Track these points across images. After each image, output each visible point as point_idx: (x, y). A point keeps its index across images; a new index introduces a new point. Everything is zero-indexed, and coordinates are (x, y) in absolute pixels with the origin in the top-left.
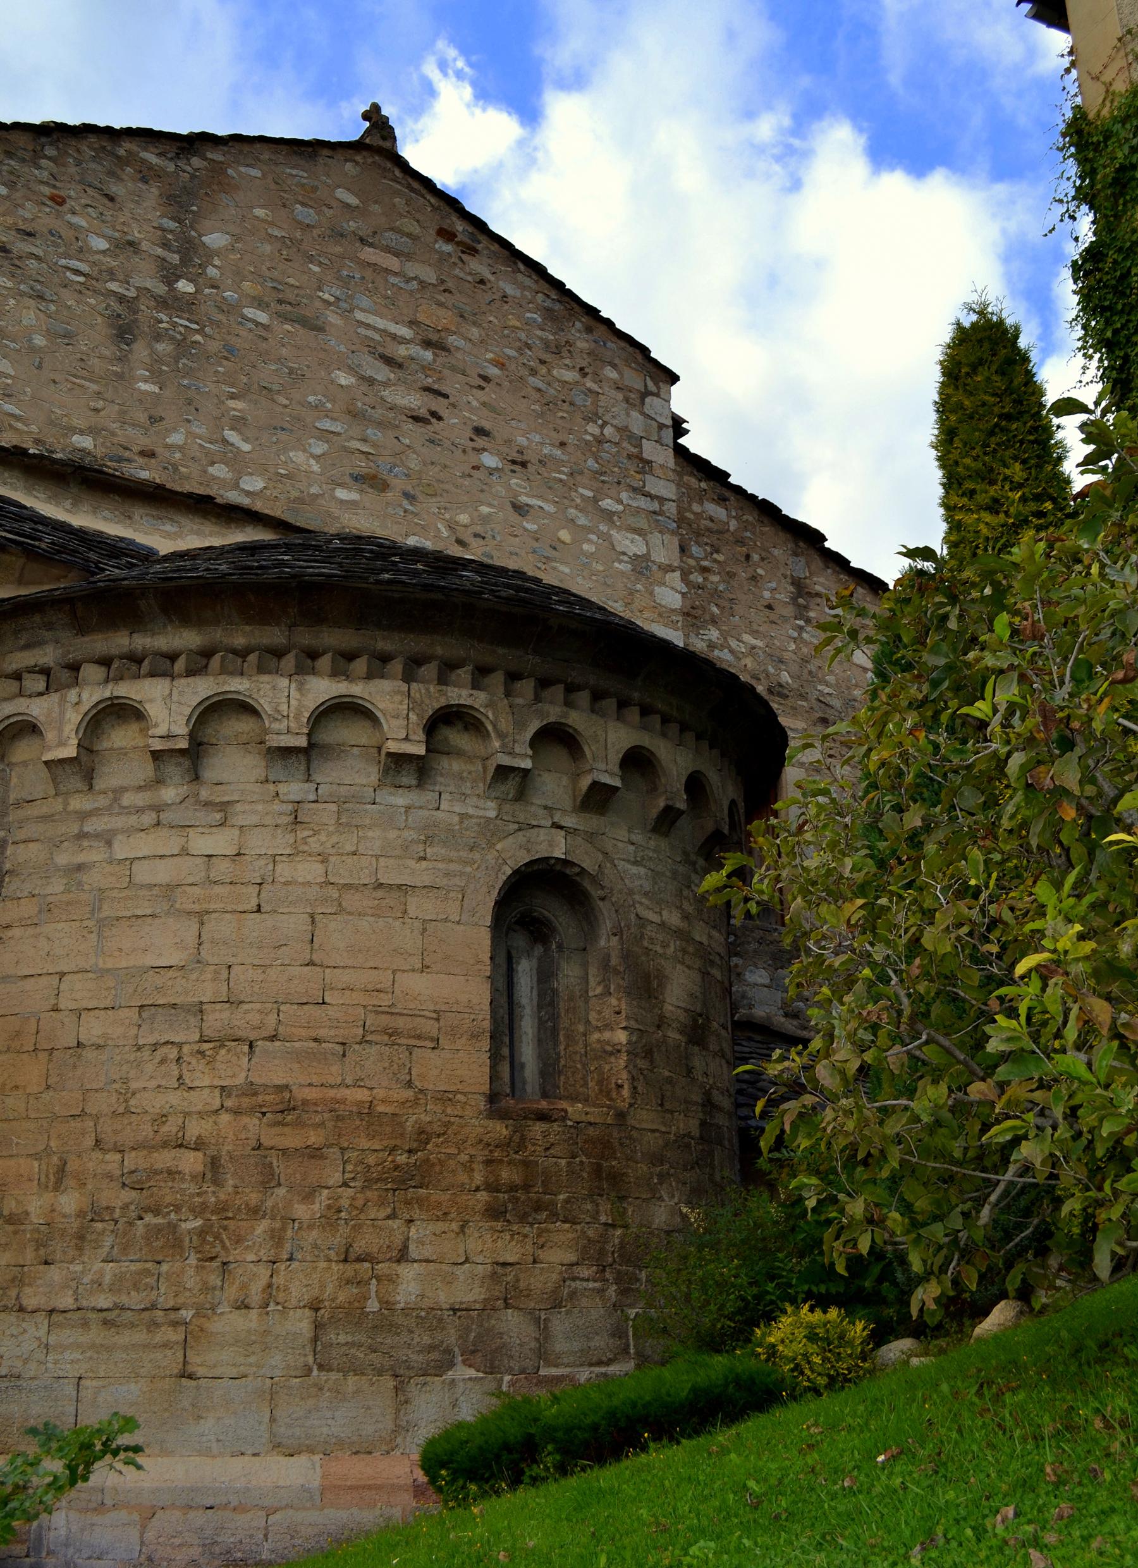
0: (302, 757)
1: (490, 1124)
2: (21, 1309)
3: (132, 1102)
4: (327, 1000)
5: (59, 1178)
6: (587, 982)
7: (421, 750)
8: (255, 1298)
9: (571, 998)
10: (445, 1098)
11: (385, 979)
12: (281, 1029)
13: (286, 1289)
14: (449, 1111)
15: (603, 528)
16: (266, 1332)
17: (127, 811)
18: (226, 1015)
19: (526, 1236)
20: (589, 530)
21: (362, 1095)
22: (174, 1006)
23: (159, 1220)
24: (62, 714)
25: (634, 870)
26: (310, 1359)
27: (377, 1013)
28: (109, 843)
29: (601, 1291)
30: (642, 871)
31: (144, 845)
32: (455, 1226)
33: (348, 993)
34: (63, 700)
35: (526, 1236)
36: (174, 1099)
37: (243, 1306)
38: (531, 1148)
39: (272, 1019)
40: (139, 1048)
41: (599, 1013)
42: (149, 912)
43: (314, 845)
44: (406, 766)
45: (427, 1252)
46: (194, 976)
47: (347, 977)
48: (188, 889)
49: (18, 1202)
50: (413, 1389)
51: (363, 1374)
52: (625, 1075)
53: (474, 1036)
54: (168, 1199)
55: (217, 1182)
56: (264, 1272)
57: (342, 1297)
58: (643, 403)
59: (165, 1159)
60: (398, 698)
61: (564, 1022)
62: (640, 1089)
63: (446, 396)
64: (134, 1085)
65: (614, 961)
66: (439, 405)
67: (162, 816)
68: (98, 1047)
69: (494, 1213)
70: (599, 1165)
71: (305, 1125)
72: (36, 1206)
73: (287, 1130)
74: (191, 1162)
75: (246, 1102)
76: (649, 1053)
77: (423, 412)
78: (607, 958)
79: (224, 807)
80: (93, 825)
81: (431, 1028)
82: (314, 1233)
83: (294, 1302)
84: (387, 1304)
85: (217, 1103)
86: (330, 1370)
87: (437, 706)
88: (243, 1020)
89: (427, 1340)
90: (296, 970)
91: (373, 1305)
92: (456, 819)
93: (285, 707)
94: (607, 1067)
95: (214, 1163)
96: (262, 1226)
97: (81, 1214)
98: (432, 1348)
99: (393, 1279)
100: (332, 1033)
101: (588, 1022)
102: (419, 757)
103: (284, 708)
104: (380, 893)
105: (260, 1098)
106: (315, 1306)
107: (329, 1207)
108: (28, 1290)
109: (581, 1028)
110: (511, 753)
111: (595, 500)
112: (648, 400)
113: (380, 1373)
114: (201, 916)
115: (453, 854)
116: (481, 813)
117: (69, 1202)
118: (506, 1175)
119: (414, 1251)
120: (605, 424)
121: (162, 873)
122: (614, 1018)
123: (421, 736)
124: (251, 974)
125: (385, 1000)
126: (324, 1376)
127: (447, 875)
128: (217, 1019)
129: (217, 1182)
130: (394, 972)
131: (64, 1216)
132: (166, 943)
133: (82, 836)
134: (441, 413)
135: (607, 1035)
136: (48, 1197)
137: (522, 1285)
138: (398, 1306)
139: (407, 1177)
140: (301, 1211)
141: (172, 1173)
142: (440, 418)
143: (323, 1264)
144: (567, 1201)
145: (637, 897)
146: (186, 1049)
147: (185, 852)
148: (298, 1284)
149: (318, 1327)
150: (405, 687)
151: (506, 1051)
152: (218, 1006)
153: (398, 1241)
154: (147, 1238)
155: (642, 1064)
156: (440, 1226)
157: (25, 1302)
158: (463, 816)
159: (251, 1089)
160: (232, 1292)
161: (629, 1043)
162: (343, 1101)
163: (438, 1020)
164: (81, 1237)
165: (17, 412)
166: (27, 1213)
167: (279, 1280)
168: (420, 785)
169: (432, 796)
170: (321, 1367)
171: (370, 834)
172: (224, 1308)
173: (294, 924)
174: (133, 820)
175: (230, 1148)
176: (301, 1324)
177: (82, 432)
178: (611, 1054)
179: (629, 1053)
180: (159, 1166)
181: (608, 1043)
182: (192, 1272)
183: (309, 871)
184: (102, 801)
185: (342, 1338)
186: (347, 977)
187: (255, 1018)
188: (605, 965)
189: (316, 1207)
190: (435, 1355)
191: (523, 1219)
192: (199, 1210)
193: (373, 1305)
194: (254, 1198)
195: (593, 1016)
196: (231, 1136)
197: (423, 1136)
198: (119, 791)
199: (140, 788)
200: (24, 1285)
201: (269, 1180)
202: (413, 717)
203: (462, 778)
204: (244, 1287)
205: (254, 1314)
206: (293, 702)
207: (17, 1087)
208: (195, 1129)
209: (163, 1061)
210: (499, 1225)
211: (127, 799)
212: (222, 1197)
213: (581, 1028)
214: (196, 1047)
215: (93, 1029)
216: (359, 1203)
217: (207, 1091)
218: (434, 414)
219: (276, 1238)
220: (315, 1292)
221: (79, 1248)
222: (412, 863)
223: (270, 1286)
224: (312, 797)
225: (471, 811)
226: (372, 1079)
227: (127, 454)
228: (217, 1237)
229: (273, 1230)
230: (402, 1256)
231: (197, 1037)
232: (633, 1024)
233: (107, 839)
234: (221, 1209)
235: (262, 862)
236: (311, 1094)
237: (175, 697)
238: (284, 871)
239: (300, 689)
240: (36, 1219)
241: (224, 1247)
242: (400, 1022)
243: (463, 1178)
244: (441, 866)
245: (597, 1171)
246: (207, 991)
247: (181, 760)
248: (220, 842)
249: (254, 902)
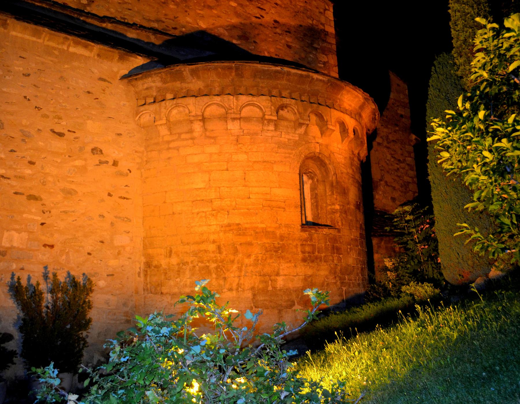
0: (238, 121)
1: (302, 234)
2: (162, 293)
3: (192, 230)
4: (251, 197)
5: (170, 254)
6: (326, 191)
7: (276, 118)
8: (234, 286)
9: (321, 196)
10: (287, 226)
11: (267, 190)
12: (237, 206)
13: (244, 284)
14: (289, 230)
15: (314, 52)
16: (239, 297)
17: (184, 140)
18: (219, 202)
19: (314, 267)
20: (310, 53)
21: (263, 226)
22: (203, 200)
23: (203, 264)
24: (160, 110)
25: (339, 156)
26: (252, 305)
27: (266, 200)
28: (178, 150)
29: (335, 283)
30: (342, 156)
31: (189, 151)
32: (293, 265)
33: (257, 195)
34: (160, 106)
35: (314, 267)
36: (205, 228)
37: (231, 290)
38: (314, 241)
39: (234, 203)
40: (193, 213)
41: (330, 200)
42: (192, 171)
43: (244, 149)
44: (271, 123)
45: (286, 272)
46: (208, 191)
47: (256, 190)
48: (205, 164)
49: (158, 261)
50: (283, 313)
51: (268, 308)
52: (339, 219)
53: (296, 207)
54: (205, 259)
55: (220, 253)
56: (237, 280)
57: (261, 286)
58: (325, 13)
59: (203, 247)
60: (268, 102)
61: (320, 203)
62: (344, 223)
63: (265, 10)
64: (193, 225)
65: (334, 185)
66: (263, 13)
67: (195, 141)
68: (179, 214)
69: (304, 260)
70: (333, 246)
71: (246, 235)
72: (164, 262)
73: (240, 237)
74: (212, 247)
75: (227, 229)
76: (345, 212)
77: (258, 15)
78: (332, 183)
79: (214, 138)
80: (172, 145)
81: (283, 205)
82: (251, 267)
83: (246, 288)
84: (274, 288)
85: (218, 229)
86: (258, 308)
87: (280, 104)
88: (226, 203)
89: (287, 298)
90: (240, 188)
91: (270, 288)
92: (287, 140)
93: (232, 105)
94: (333, 217)
95: (219, 248)
96: (235, 267)
97: (178, 264)
98: (289, 300)
99: (276, 281)
100: (253, 207)
101: (326, 203)
102: (275, 120)
103: (232, 105)
104: (265, 164)
105: (232, 227)
106: (253, 288)
107: (255, 259)
108: (163, 288)
109: (325, 205)
110: (303, 119)
111: (312, 44)
112: (326, 12)
113: (273, 308)
114: (209, 172)
115: (286, 151)
116: (294, 138)
117: (174, 261)
118: (307, 249)
119: (281, 272)
120: (314, 19)
121: (196, 159)
122: (335, 201)
123: (275, 114)
124: (226, 189)
125: (268, 197)
126: (257, 309)
127: (285, 158)
128: (217, 203)
129: (220, 253)
130: (271, 188)
131: (173, 265)
132: (199, 182)
133: (169, 149)
134: (263, 15)
135: (333, 207)
136: (167, 260)
137: (313, 281)
138: (278, 289)
139: (278, 250)
140: (247, 261)
141: (206, 251)
142: (263, 17)
143: (254, 277)
144: (325, 256)
145: (340, 164)
146: (208, 213)
147: (203, 152)
148: (247, 283)
149: (254, 295)
150: (269, 98)
151: (303, 212)
152: (217, 200)
153: (276, 269)
154: (200, 271)
155: (344, 215)
156: (289, 265)
157: (163, 291)
158: (289, 140)
159: (229, 225)
160: (227, 286)
161: (340, 209)
162: (257, 228)
163: (285, 202)
164: (179, 271)
165: (37, 58)
166: (161, 265)
167: (242, 282)
168: (276, 130)
169: (279, 133)
170: (256, 307)
171: (261, 145)
172: (225, 290)
173: (238, 174)
174: (185, 143)
175: (224, 243)
176: (249, 295)
177: (153, 21)
178: (335, 213)
179: (340, 212)
180: (202, 249)
181: (334, 209)
182: (214, 280)
183: (242, 157)
184: (175, 137)
185: (262, 298)
186: (256, 190)
187: (228, 203)
188: (332, 186)
189: (252, 259)
190: (290, 303)
191: (313, 261)
192: (216, 261)
193: (270, 288)
194: (232, 257)
195: (328, 201)
196: (224, 239)
197: (282, 238)
198: (180, 134)
199: (187, 133)
200: (162, 286)
201: (236, 251)
202: (273, 108)
203: (288, 127)
204: (231, 284)
205: (234, 292)
206: (235, 104)
207: (154, 227)
208: (212, 237)
209: (201, 217)
210: (306, 264)
211: (183, 136)
212: (222, 257)
213: (325, 205)
214: (211, 212)
215: (178, 208)
216: (264, 258)
217: (215, 226)
218: (261, 16)
219: (240, 269)
220: (252, 285)
221: (179, 275)
222: (274, 154)
223: (238, 284)
224: (242, 134)
225: (291, 138)
226: (263, 221)
227: (168, 28)
228: (222, 270)
229: (238, 267)
230: (278, 274)
231: (210, 209)
232: (341, 204)
233: (177, 149)
234: (222, 261)
235: (227, 155)
236: (247, 226)
237: (197, 103)
238: (235, 157)
239: (237, 100)
240: (164, 266)
241: (224, 272)
242: (273, 204)
243: (295, 250)
244: (283, 155)
245: (333, 247)
246: (213, 195)
247: (200, 123)
248: (214, 149)
249: (226, 167)
